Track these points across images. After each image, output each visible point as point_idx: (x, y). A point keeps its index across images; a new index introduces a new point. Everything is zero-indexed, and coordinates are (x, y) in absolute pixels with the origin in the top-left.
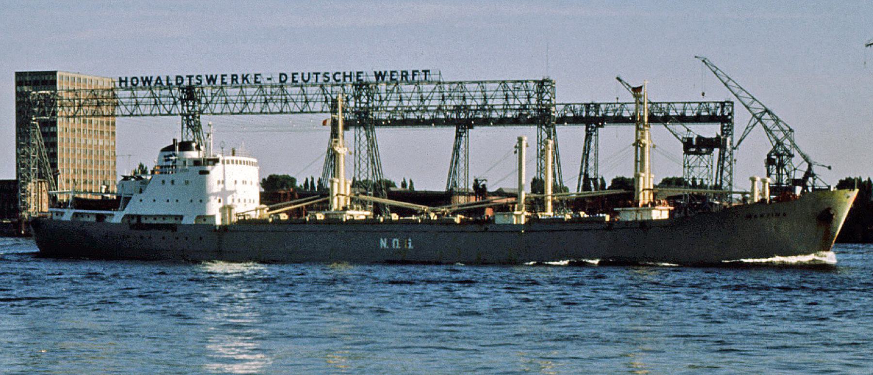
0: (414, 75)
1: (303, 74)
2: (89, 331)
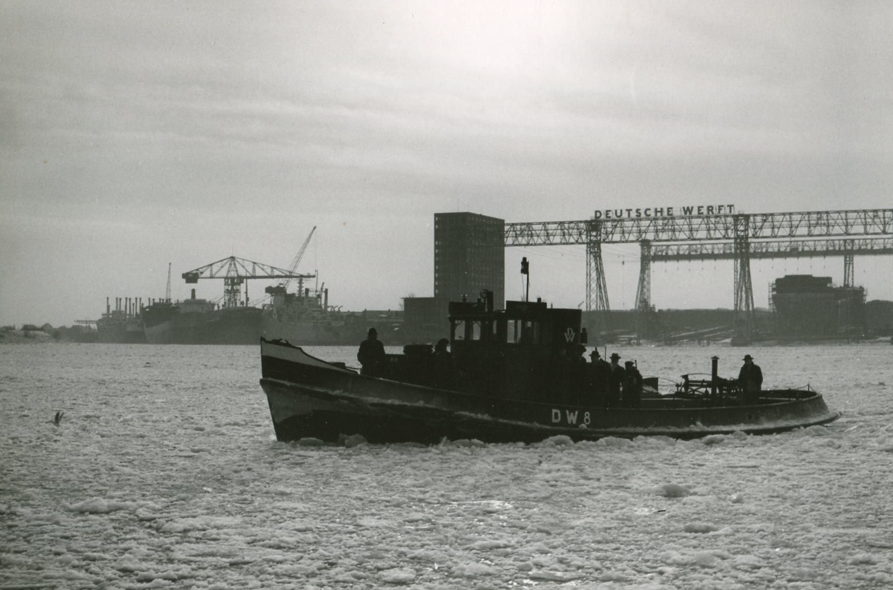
0: (720, 209)
1: (616, 211)
2: (478, 494)
